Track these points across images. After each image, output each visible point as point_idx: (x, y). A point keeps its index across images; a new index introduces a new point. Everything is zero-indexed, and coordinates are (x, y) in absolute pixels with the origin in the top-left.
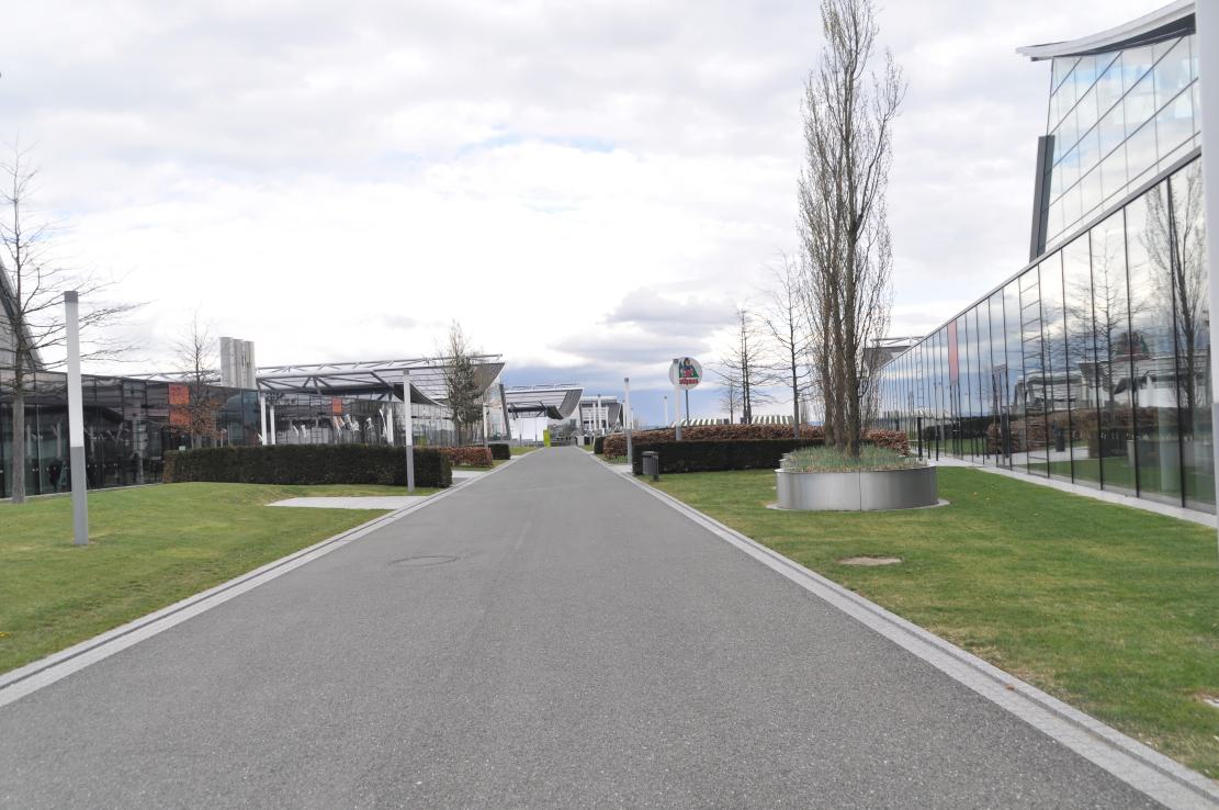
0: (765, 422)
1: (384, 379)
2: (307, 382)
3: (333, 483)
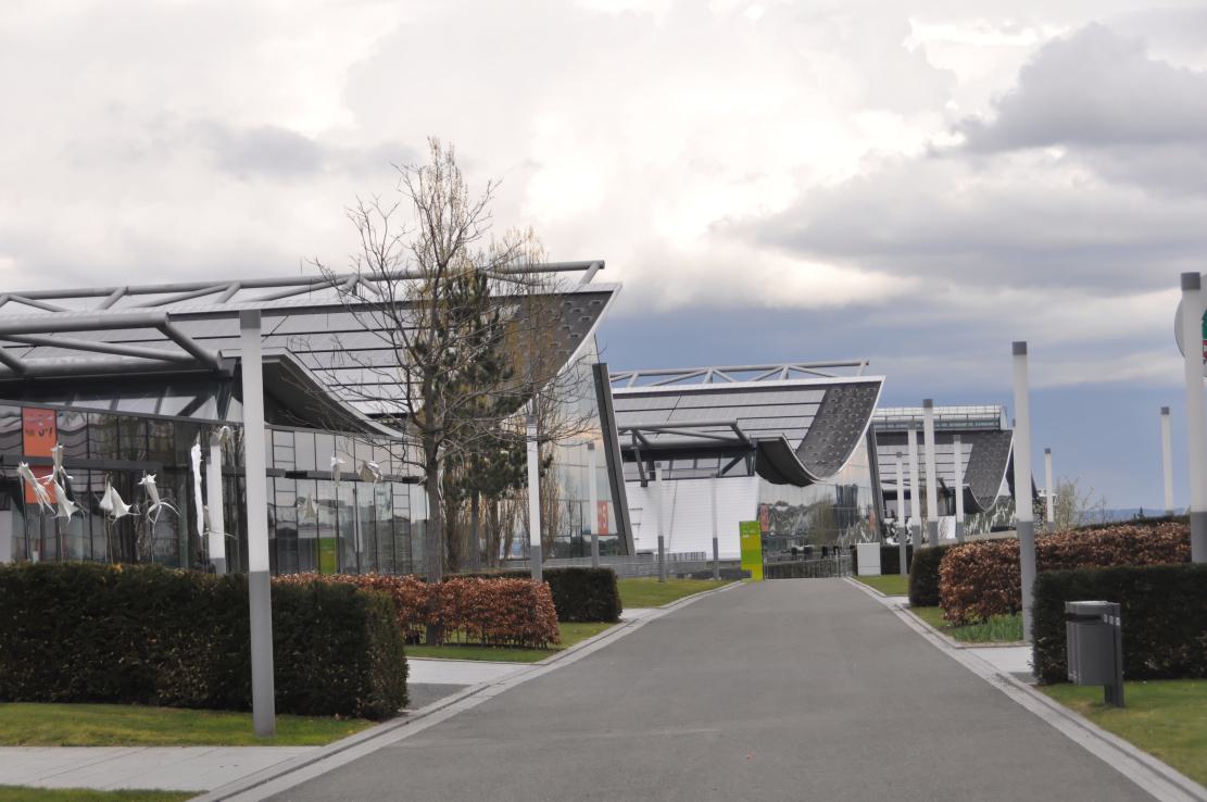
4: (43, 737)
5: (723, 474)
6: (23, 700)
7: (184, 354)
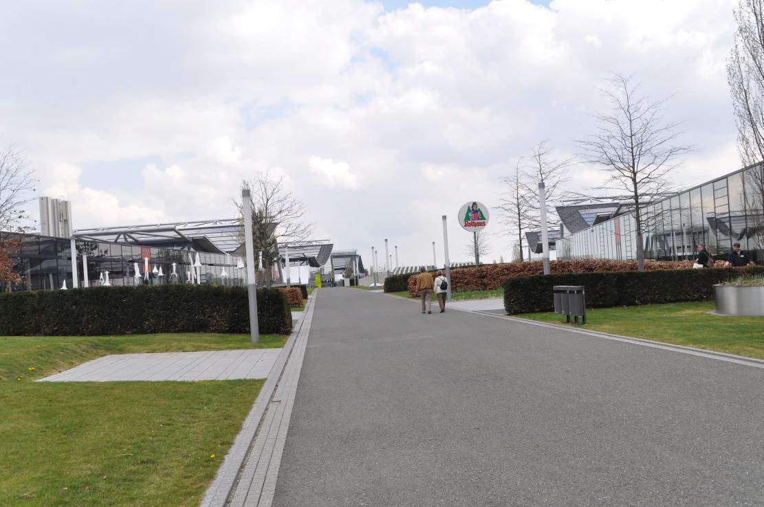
0: (228, 284)
1: (183, 233)
2: (118, 238)
3: (154, 332)
4: (175, 348)
5: (301, 265)
6: (162, 333)
7: (179, 236)
